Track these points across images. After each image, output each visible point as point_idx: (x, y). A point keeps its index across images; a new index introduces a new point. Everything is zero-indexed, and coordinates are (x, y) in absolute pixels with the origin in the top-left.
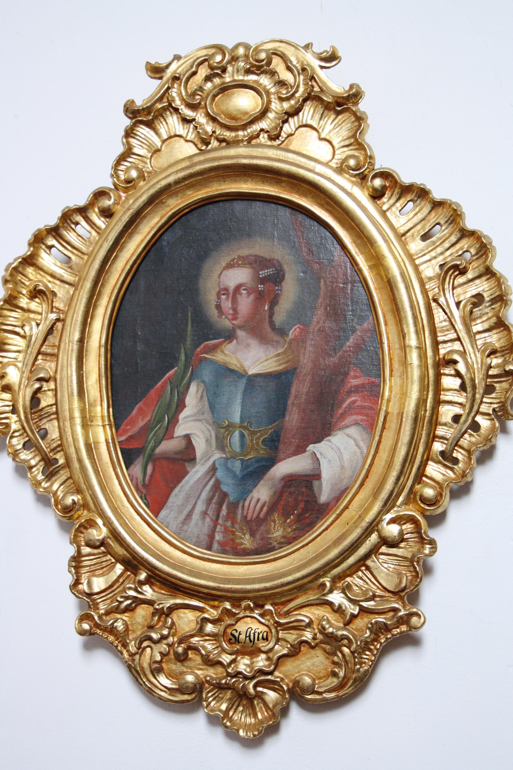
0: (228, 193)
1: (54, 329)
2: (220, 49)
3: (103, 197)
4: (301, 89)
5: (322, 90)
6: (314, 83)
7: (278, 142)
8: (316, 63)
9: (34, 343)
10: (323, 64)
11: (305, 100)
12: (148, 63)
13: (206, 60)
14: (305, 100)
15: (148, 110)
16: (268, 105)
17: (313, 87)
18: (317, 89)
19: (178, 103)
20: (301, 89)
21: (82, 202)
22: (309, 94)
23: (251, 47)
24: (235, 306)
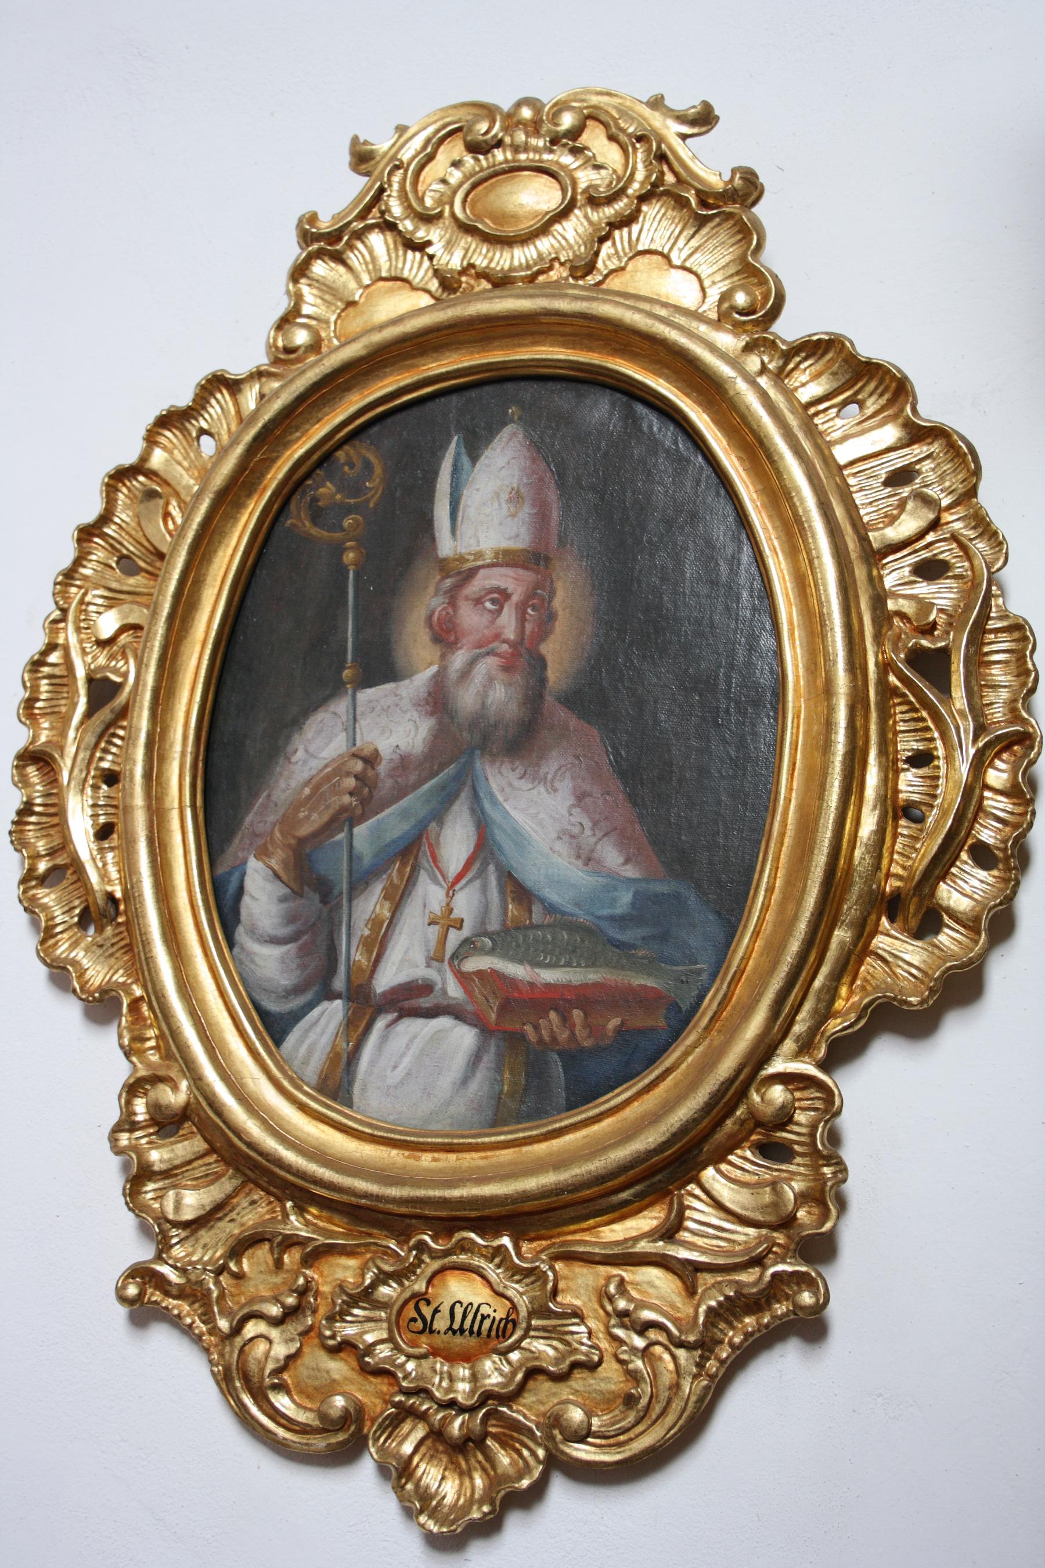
0: (611, 370)
1: (264, 380)
2: (488, 111)
3: (426, 750)
4: (640, 175)
5: (680, 180)
6: (665, 168)
7: (591, 280)
8: (672, 129)
9: (435, 122)
10: (686, 130)
11: (644, 198)
12: (355, 140)
13: (459, 130)
14: (644, 198)
15: (334, 237)
16: (516, 242)
17: (662, 173)
18: (670, 178)
19: (396, 209)
20: (640, 175)
21: (987, 497)
22: (655, 185)
23: (544, 105)
24: (834, 984)
